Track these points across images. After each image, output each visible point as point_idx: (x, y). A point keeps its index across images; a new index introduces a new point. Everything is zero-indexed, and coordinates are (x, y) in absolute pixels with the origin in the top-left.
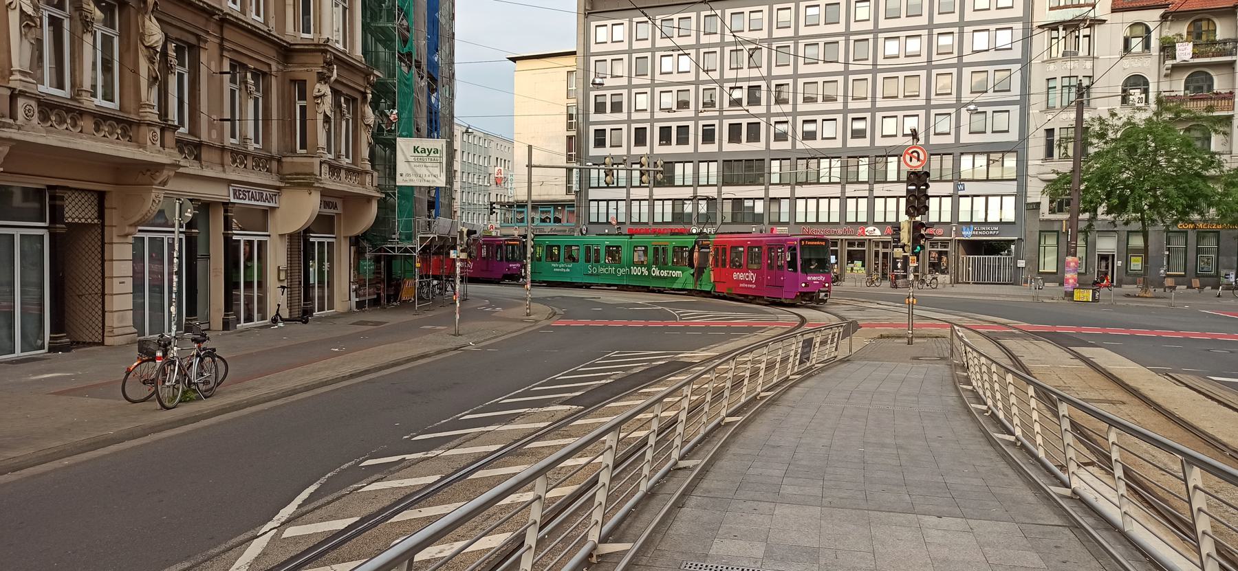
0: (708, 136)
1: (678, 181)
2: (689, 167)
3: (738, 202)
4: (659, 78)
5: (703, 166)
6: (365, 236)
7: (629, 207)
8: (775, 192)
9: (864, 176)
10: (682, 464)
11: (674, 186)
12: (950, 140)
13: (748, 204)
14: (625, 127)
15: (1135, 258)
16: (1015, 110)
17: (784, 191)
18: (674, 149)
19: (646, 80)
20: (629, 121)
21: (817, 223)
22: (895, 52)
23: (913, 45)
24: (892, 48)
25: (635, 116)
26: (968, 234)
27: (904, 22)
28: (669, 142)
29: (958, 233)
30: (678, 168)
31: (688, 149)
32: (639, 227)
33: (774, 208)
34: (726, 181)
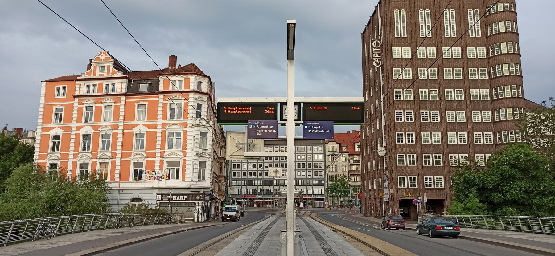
0: (260, 174)
1: (253, 185)
3: (267, 190)
5: (259, 181)
6: (223, 201)
7: (313, 191)
8: (275, 187)
11: (252, 185)
12: (311, 177)
13: (269, 190)
14: (241, 172)
15: (117, 186)
17: (277, 187)
18: (251, 177)
20: (242, 170)
22: (300, 158)
23: (303, 157)
26: (315, 197)
29: (313, 197)
30: (253, 181)
31: (256, 177)
32: (249, 195)
33: (275, 191)
34: (265, 184)
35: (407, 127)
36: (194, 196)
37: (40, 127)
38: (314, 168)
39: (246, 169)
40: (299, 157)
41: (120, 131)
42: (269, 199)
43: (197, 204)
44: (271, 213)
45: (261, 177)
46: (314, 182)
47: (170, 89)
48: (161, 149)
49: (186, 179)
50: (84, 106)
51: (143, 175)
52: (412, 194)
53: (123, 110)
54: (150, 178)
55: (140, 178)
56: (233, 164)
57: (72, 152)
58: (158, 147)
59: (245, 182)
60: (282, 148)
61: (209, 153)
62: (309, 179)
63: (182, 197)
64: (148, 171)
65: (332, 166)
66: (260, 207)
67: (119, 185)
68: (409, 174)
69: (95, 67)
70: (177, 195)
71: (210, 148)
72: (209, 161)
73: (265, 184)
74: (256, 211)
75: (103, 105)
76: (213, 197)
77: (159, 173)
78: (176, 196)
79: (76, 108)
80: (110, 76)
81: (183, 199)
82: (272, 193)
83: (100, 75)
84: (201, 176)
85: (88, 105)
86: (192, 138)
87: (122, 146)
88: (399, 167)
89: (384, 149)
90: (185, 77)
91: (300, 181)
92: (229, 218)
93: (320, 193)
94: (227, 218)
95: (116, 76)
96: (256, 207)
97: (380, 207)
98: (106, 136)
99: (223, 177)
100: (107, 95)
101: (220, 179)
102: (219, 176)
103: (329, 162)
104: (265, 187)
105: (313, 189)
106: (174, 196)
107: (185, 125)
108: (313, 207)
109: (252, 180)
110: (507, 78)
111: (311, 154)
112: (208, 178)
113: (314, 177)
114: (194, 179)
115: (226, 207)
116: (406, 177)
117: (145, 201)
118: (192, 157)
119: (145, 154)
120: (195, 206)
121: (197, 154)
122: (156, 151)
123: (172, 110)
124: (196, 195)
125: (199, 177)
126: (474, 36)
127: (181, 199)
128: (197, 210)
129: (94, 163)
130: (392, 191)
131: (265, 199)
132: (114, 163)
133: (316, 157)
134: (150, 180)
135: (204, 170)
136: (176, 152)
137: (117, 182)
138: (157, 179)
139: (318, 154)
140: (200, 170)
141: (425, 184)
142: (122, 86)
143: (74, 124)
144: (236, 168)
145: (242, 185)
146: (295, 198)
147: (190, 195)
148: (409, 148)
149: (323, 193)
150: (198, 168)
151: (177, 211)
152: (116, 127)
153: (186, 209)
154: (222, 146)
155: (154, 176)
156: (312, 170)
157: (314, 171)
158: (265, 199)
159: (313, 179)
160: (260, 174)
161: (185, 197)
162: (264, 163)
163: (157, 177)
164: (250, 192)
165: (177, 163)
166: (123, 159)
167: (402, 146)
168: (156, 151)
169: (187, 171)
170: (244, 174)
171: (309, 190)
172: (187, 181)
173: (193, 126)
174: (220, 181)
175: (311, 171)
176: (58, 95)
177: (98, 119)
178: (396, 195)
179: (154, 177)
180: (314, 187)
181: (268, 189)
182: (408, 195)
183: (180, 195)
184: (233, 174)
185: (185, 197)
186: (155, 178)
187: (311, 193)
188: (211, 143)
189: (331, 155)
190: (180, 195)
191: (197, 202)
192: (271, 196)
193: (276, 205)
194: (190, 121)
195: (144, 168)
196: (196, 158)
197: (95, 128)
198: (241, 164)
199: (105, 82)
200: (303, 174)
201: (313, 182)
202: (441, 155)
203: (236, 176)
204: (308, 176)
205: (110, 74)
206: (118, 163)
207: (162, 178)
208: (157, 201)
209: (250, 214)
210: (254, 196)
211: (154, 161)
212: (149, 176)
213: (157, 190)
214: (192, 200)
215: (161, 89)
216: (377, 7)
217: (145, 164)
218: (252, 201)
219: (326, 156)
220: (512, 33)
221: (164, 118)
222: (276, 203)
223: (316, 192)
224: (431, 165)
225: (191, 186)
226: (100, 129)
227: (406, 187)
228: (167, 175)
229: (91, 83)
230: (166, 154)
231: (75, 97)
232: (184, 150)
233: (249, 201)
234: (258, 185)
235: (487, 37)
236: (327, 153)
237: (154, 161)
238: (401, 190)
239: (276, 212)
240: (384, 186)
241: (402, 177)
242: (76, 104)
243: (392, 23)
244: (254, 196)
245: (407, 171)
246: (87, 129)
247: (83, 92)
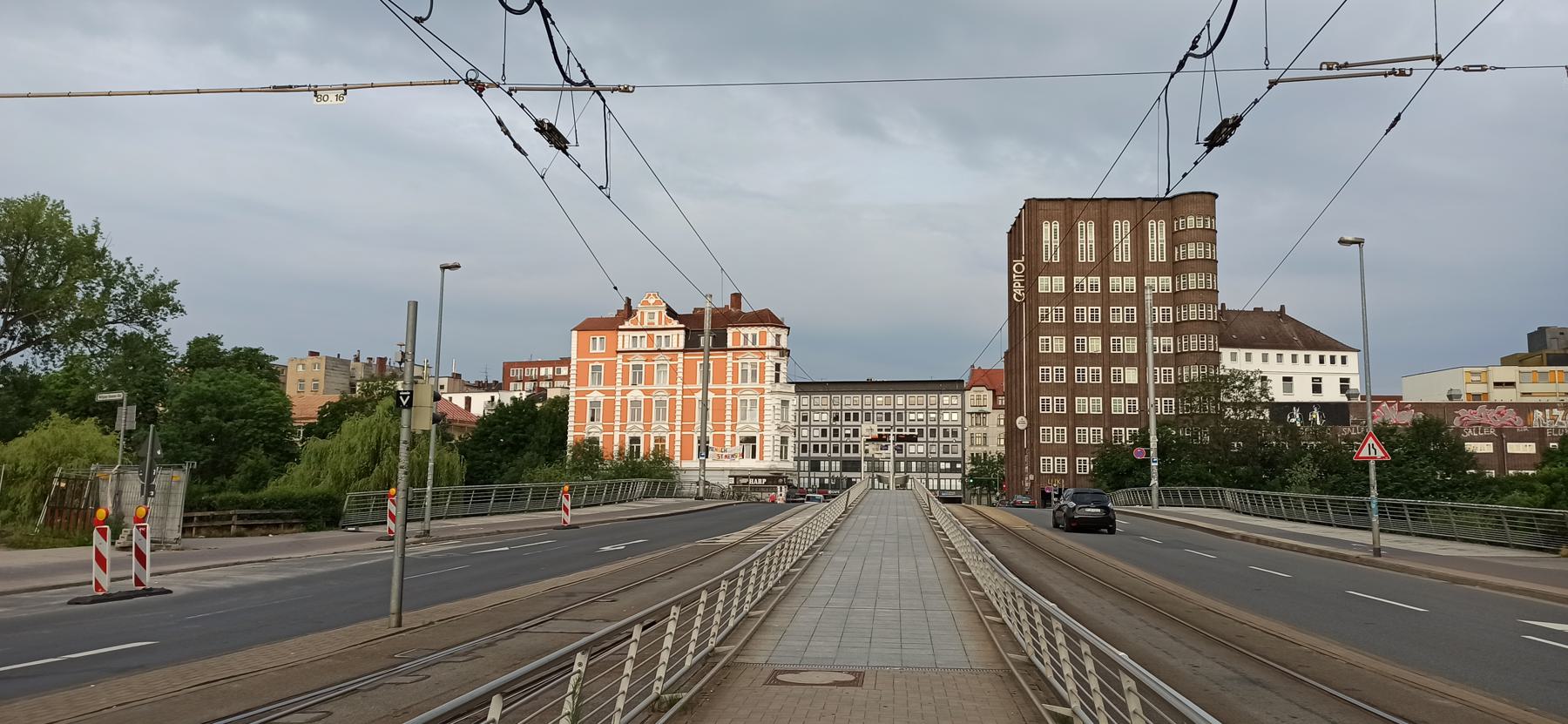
0: (836, 450)
1: (822, 469)
2: (827, 463)
4: (813, 423)
5: (833, 462)
7: (939, 483)
9: (902, 470)
10: (752, 613)
13: (853, 480)
16: (960, 445)
18: (820, 454)
19: (807, 423)
21: (951, 490)
24: (912, 416)
25: (802, 439)
26: (944, 495)
27: (916, 407)
28: (817, 452)
29: (940, 494)
30: (822, 463)
31: (825, 455)
37: (574, 390)
38: (942, 439)
39: (807, 439)
40: (912, 416)
41: (679, 398)
43: (779, 490)
45: (838, 455)
46: (942, 465)
47: (742, 345)
50: (631, 364)
53: (681, 370)
57: (618, 423)
58: (729, 418)
60: (879, 399)
62: (933, 460)
69: (642, 313)
70: (754, 477)
75: (655, 363)
77: (730, 450)
79: (620, 367)
80: (663, 326)
83: (649, 324)
84: (783, 455)
85: (635, 363)
86: (772, 408)
89: (1025, 419)
90: (760, 329)
91: (914, 464)
93: (953, 488)
95: (670, 326)
98: (660, 403)
100: (659, 351)
103: (972, 426)
104: (846, 474)
105: (939, 480)
107: (762, 391)
109: (819, 461)
110: (1194, 323)
113: (942, 455)
114: (776, 459)
120: (776, 492)
121: (779, 428)
122: (726, 423)
123: (745, 372)
125: (781, 457)
126: (1155, 260)
129: (647, 438)
132: (672, 437)
135: (786, 448)
140: (782, 447)
141: (1077, 467)
142: (678, 339)
143: (619, 387)
148: (1057, 420)
149: (959, 488)
152: (674, 392)
155: (724, 454)
156: (939, 442)
159: (940, 460)
160: (836, 450)
161: (765, 480)
162: (843, 428)
165: (753, 440)
166: (683, 433)
168: (726, 423)
171: (930, 481)
173: (772, 392)
176: (595, 348)
177: (650, 381)
180: (942, 475)
183: (758, 477)
185: (765, 480)
186: (726, 456)
187: (936, 488)
189: (976, 413)
190: (758, 477)
191: (779, 487)
194: (767, 386)
195: (711, 445)
196: (777, 432)
197: (645, 392)
199: (657, 333)
200: (921, 449)
201: (939, 465)
202: (1101, 429)
205: (663, 323)
206: (678, 437)
211: (724, 436)
215: (730, 344)
216: (1020, 216)
219: (967, 415)
220: (1211, 260)
221: (735, 381)
223: (945, 485)
224: (1087, 442)
226: (654, 394)
229: (638, 334)
231: (618, 352)
235: (1174, 263)
237: (724, 436)
241: (1046, 458)
242: (620, 362)
243: (1039, 241)
245: (1054, 450)
246: (636, 394)
247: (628, 346)
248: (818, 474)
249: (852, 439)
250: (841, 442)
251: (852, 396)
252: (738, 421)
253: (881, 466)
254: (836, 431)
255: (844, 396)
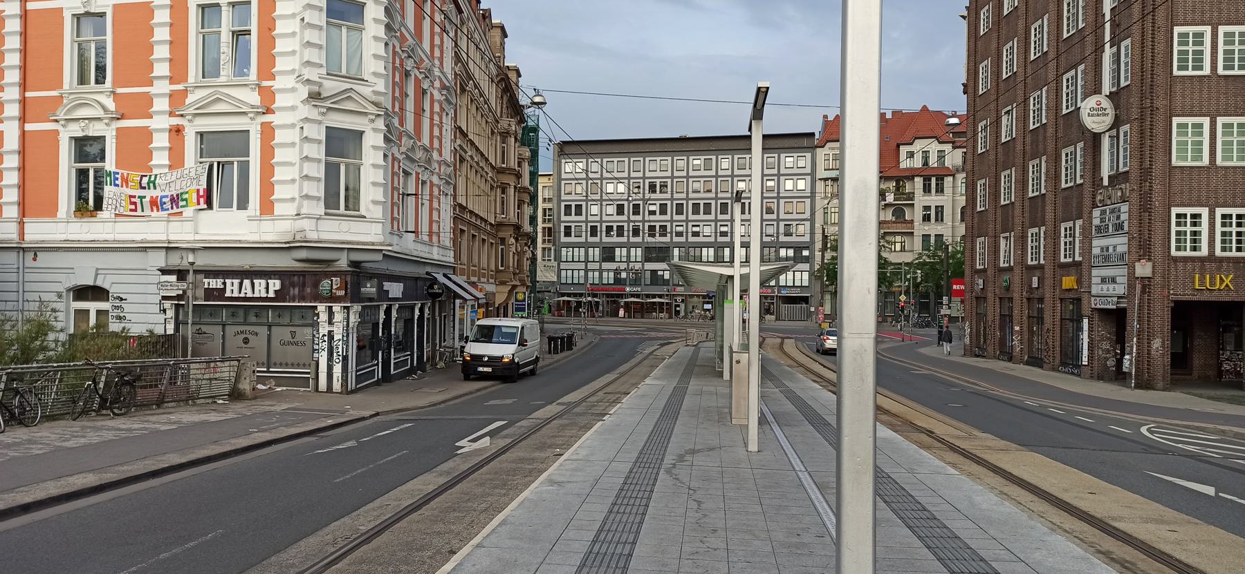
0: (636, 232)
1: (617, 259)
3: (654, 272)
18: (615, 239)
20: (587, 222)
25: (590, 218)
26: (784, 293)
30: (618, 250)
31: (624, 239)
32: (608, 287)
34: (647, 259)
35: (1224, 6)
36: (309, 280)
39: (598, 218)
42: (660, 296)
43: (324, 317)
44: (660, 339)
46: (783, 252)
48: (172, 80)
49: (279, 209)
51: (108, 190)
52: (1227, 281)
54: (135, 204)
55: (99, 205)
56: (563, 204)
58: (161, 69)
59: (595, 253)
61: (374, 98)
63: (260, 284)
64: (125, 173)
65: (833, 210)
66: (634, 318)
67: (22, 233)
68: (1221, 201)
71: (375, 74)
72: (375, 130)
73: (647, 259)
74: (621, 329)
76: (436, 287)
78: (236, 282)
81: (264, 295)
82: (666, 283)
87: (24, 68)
88: (1178, 171)
89: (1106, 104)
92: (486, 369)
93: (798, 283)
94: (481, 369)
96: (624, 317)
97: (1058, 338)
99: (512, 228)
101: (501, 235)
102: (500, 225)
104: (650, 266)
106: (228, 282)
108: (777, 319)
109: (614, 248)
111: (776, 178)
112: (371, 206)
113: (782, 239)
114: (307, 208)
115: (478, 326)
116: (1205, 212)
117: (122, 299)
118: (297, 112)
119: (111, 105)
120: (315, 325)
121: (315, 96)
122: (152, 90)
124: (318, 277)
127: (257, 295)
128: (326, 338)
130: (1143, 269)
131: (648, 296)
133: (789, 185)
134: (135, 210)
136: (233, 92)
137: (9, 220)
138: (163, 209)
139: (795, 178)
144: (571, 215)
145: (586, 261)
146: (760, 296)
147: (296, 278)
149: (806, 283)
150: (319, 161)
151: (246, 341)
153: (280, 333)
154: (508, 133)
155: (149, 194)
157: (782, 224)
158: (648, 296)
161: (275, 284)
163: (162, 197)
164: (609, 278)
167: (1197, 84)
168: (152, 90)
169: (280, 174)
170: (594, 231)
172: (283, 218)
174: (503, 240)
175: (775, 223)
178: (1163, 287)
179: (148, 199)
181: (656, 271)
182: (1212, 283)
183: (252, 274)
184: (562, 229)
185: (275, 284)
186: (154, 203)
188: (382, 52)
190: (252, 274)
191: (321, 308)
192: (663, 290)
193: (678, 313)
195: (110, 164)
196: (307, 111)
198: (584, 204)
201: (777, 252)
203: (571, 236)
204: (766, 236)
207: (181, 203)
208: (164, 298)
209: (601, 338)
210: (619, 290)
211: (147, 134)
212: (131, 197)
213: (163, 253)
214: (302, 299)
217: (114, 145)
218: (614, 302)
219: (818, 183)
222: (678, 309)
225: (298, 238)
227: (1204, 251)
228: (201, 193)
230: (191, 98)
232: (265, 83)
233: (608, 301)
234: (631, 257)
236: (821, 173)
237: (147, 134)
238: (1180, 265)
239: (676, 335)
240: (1096, 251)
244: (619, 290)
248: (613, 266)
249: (658, 217)
250: (644, 221)
251: (658, 159)
252: (191, 79)
253: (698, 253)
254: (636, 207)
255: (647, 159)
